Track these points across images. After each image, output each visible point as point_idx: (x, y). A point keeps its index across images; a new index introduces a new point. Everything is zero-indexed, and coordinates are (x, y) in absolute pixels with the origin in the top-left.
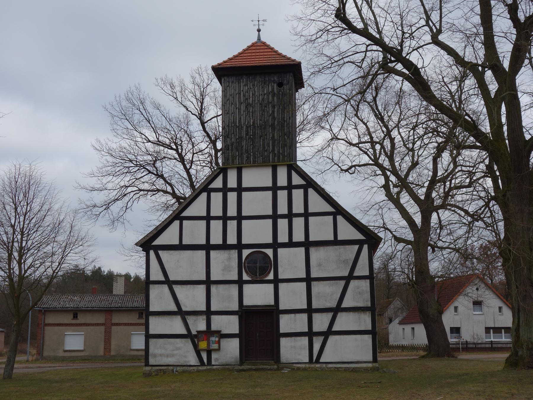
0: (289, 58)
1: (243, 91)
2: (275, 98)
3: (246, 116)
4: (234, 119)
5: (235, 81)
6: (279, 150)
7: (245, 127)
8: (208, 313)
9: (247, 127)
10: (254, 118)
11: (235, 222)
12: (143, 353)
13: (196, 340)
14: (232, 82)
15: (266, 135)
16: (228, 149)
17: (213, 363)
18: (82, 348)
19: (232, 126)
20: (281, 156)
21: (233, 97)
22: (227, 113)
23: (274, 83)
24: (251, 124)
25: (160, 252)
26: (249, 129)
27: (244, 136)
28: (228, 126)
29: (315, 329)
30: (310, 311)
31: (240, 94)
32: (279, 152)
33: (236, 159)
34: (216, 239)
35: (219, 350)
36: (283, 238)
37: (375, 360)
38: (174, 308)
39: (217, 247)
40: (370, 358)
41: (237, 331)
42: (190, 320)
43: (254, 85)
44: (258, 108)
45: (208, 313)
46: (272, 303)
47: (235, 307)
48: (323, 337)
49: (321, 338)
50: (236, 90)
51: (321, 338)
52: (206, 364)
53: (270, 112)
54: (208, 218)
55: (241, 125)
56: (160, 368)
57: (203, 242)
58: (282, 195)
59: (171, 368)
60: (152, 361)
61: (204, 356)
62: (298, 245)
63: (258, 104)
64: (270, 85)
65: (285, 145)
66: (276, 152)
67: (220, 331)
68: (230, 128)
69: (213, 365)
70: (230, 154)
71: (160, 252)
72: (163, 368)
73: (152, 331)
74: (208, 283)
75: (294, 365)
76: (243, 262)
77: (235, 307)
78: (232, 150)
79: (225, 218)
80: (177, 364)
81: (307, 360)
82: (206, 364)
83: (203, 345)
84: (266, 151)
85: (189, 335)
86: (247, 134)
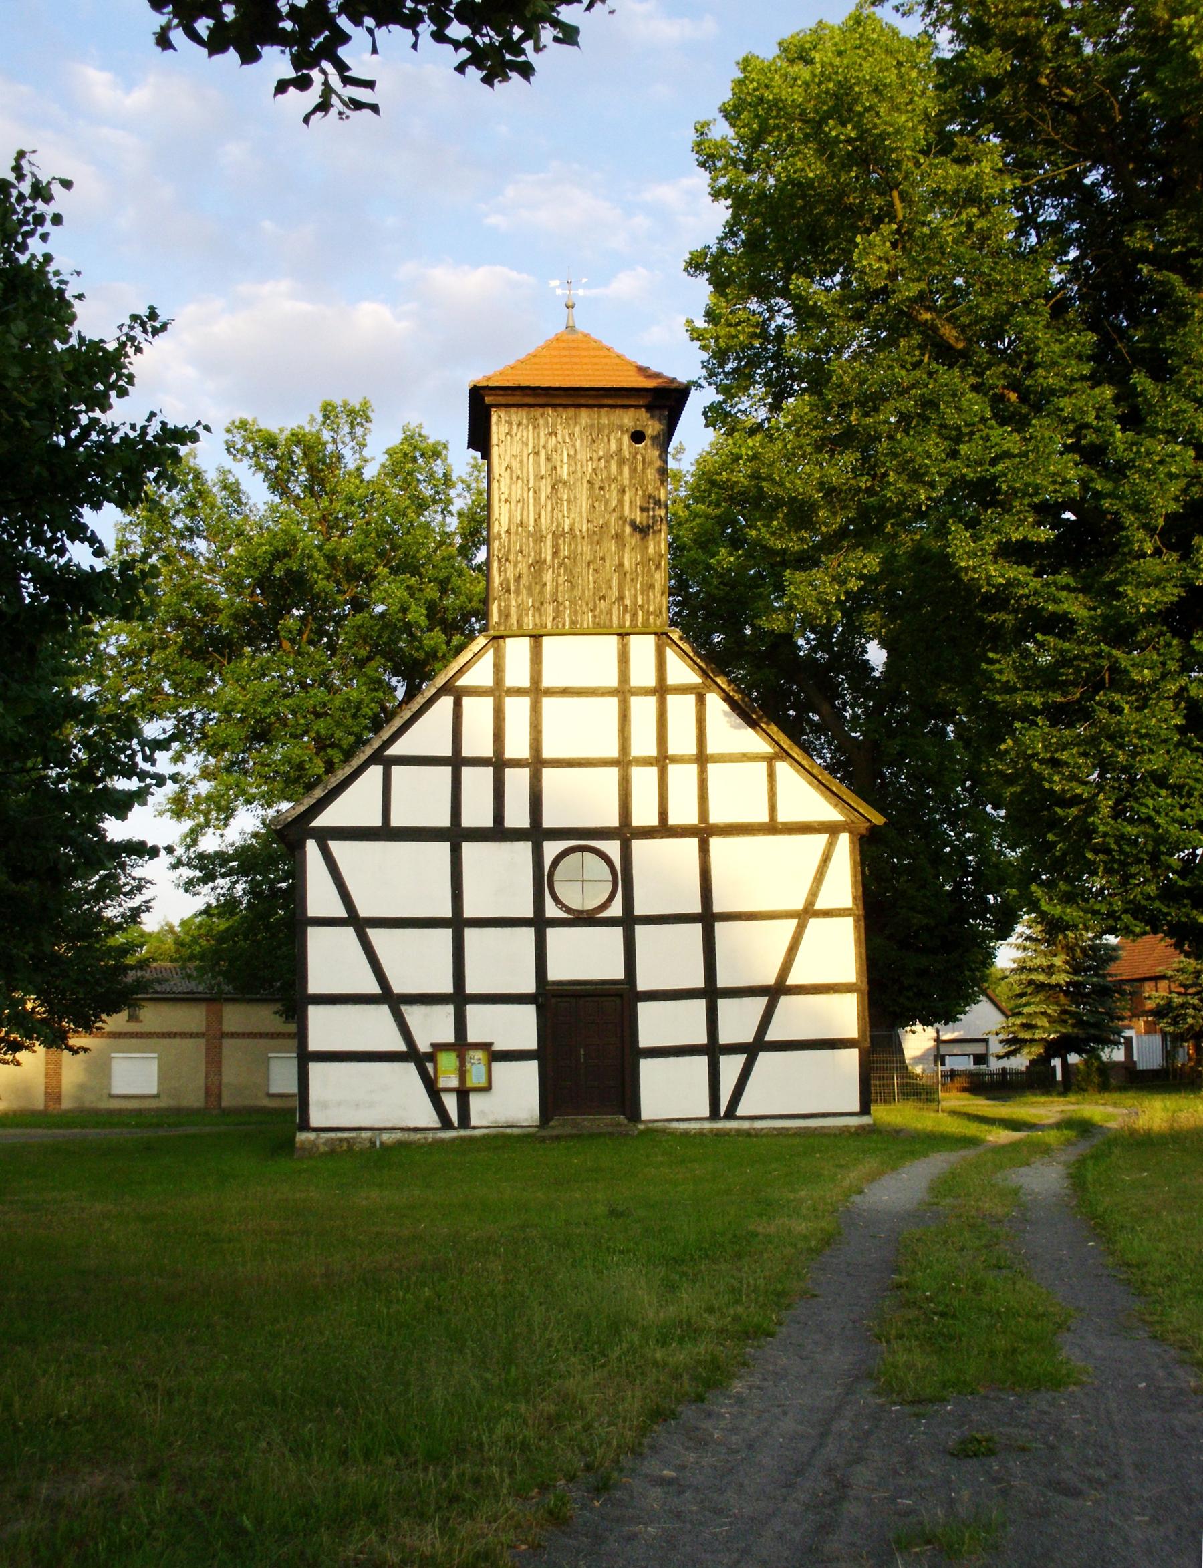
0: (657, 376)
1: (544, 447)
2: (626, 470)
3: (553, 509)
4: (522, 515)
5: (525, 421)
6: (635, 597)
7: (550, 536)
8: (460, 999)
9: (556, 537)
10: (572, 516)
11: (525, 773)
12: (296, 1103)
13: (430, 1066)
14: (519, 424)
15: (603, 559)
16: (508, 591)
17: (474, 1121)
18: (154, 1091)
19: (517, 533)
20: (640, 613)
21: (521, 462)
22: (506, 501)
23: (623, 432)
24: (567, 529)
25: (334, 845)
26: (561, 541)
27: (549, 558)
28: (508, 532)
29: (724, 1038)
30: (711, 993)
31: (537, 453)
32: (635, 603)
33: (527, 615)
34: (478, 814)
35: (488, 1088)
36: (478, 814)
37: (865, 1110)
38: (374, 988)
39: (647, 833)
40: (856, 1107)
41: (532, 1044)
42: (413, 1014)
43: (571, 435)
44: (583, 492)
45: (460, 999)
46: (619, 973)
47: (530, 987)
48: (745, 1056)
49: (740, 1059)
50: (527, 444)
51: (740, 1059)
52: (456, 1125)
53: (614, 503)
54: (457, 762)
55: (540, 531)
56: (340, 1135)
57: (445, 822)
58: (643, 709)
59: (368, 1134)
60: (316, 1119)
61: (451, 1103)
62: (516, 835)
63: (585, 481)
64: (612, 438)
65: (652, 586)
66: (628, 602)
67: (491, 1044)
68: (513, 538)
69: (474, 1128)
70: (513, 603)
71: (334, 845)
72: (346, 1135)
73: (314, 1045)
74: (458, 923)
75: (675, 1125)
76: (546, 873)
77: (530, 987)
78: (517, 592)
79: (499, 764)
80: (381, 1125)
81: (706, 1113)
82: (456, 1125)
83: (448, 1080)
84: (603, 598)
85: (412, 1055)
86: (555, 554)
